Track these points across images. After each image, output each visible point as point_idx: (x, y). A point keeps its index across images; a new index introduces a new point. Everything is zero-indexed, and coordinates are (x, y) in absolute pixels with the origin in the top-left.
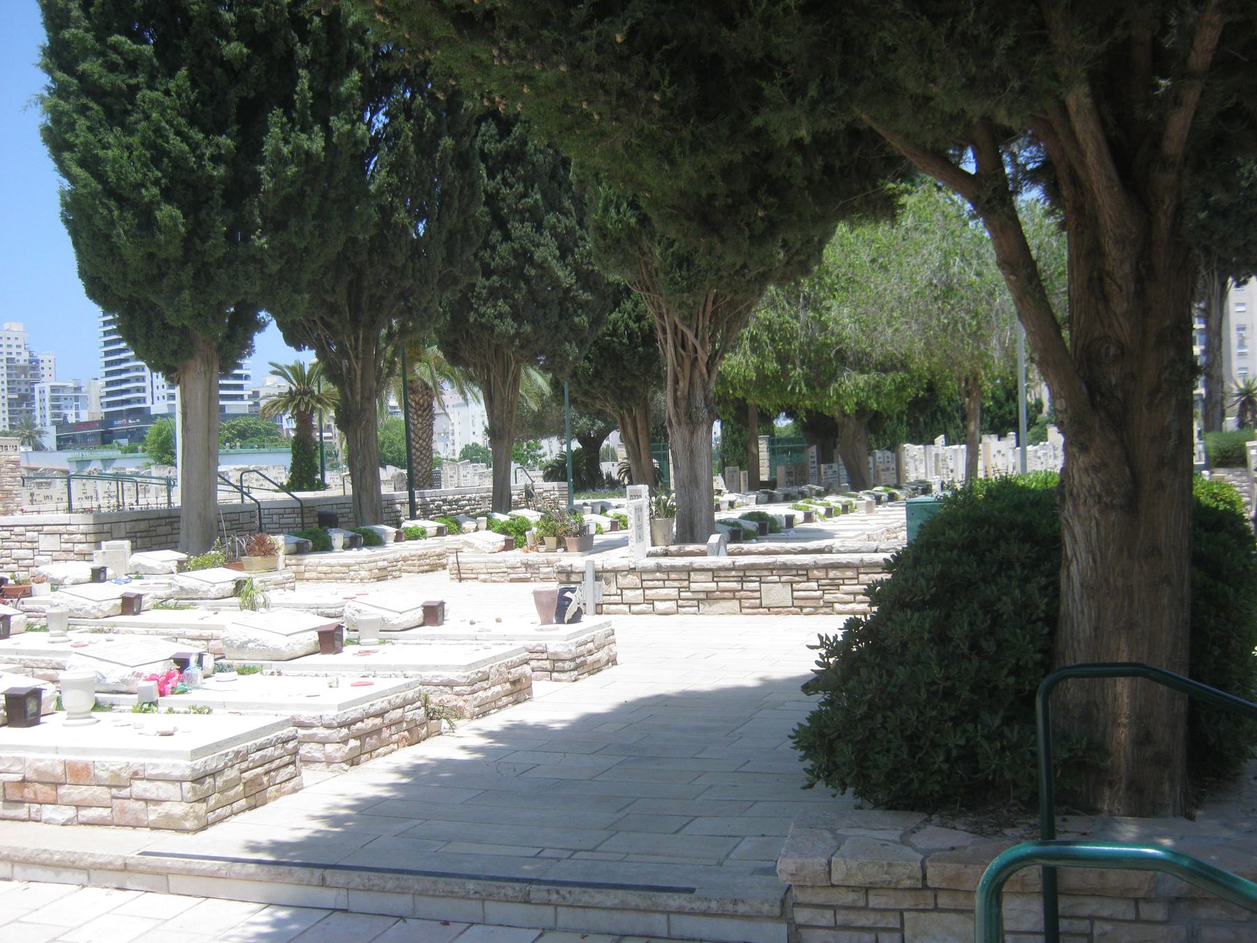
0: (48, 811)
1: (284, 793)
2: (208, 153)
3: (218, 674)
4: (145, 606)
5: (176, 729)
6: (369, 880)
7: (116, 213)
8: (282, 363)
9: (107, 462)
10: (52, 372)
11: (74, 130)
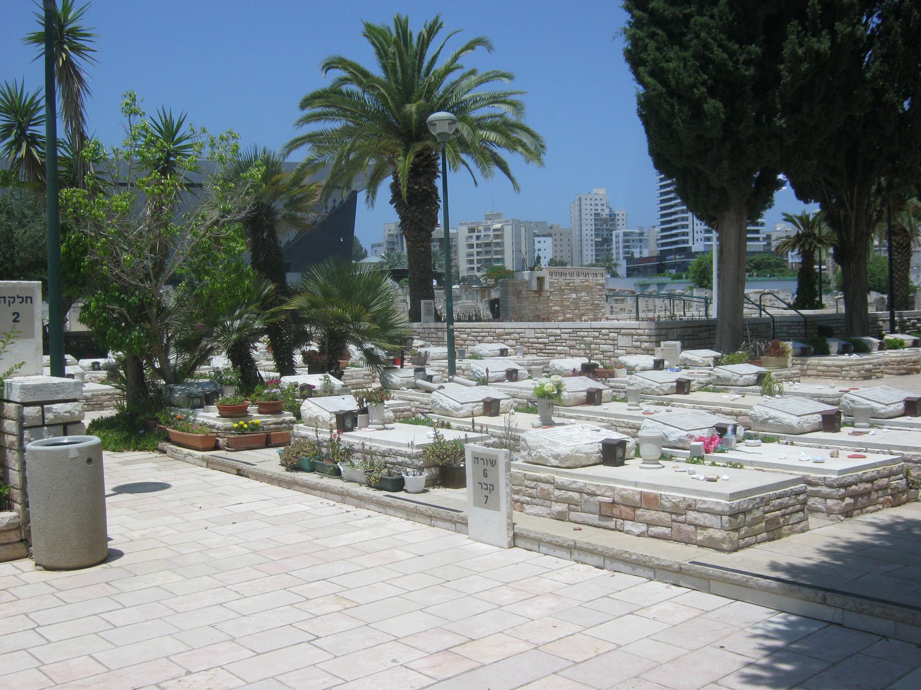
0: (628, 525)
1: (795, 532)
2: (742, 59)
3: (747, 441)
4: (693, 388)
5: (718, 477)
6: (860, 604)
7: (677, 107)
8: (791, 213)
9: (661, 285)
10: (624, 222)
11: (646, 51)
